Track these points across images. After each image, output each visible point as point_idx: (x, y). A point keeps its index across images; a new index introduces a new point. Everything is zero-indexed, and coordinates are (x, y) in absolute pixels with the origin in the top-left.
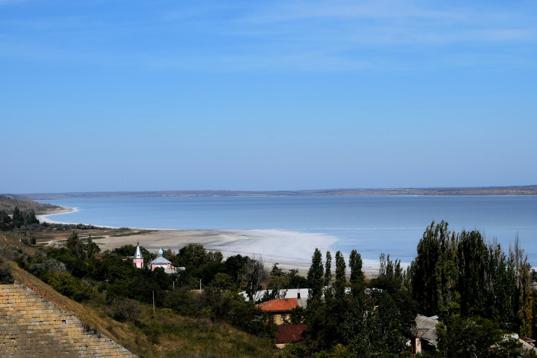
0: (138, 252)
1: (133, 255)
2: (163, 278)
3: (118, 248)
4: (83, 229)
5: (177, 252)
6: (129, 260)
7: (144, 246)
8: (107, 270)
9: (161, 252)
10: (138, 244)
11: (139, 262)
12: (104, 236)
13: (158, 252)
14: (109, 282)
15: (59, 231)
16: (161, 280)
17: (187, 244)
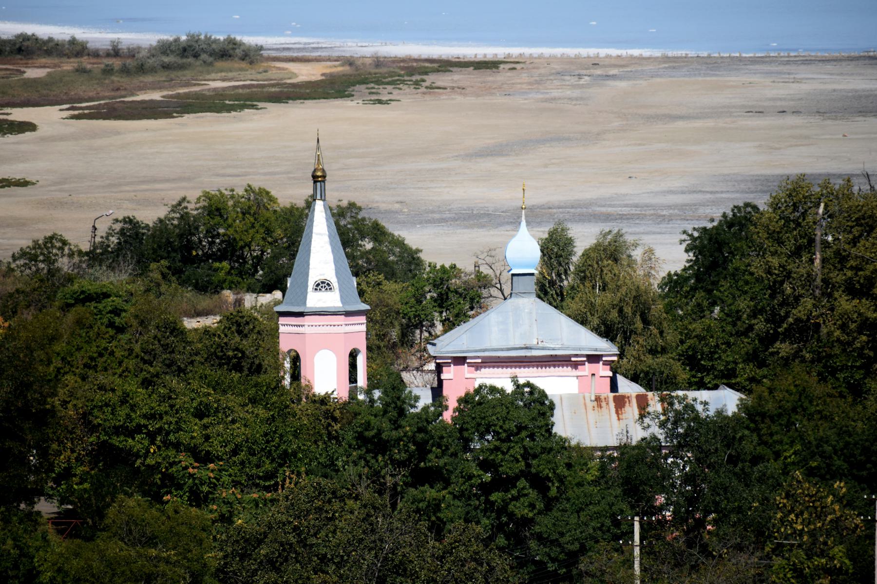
0: (321, 256)
1: (276, 282)
2: (539, 483)
3: (149, 216)
5: (671, 257)
6: (239, 323)
7: (376, 199)
8: (44, 418)
9: (524, 250)
10: (318, 179)
11: (325, 342)
12: (18, 114)
13: (494, 253)
14: (61, 522)
16: (520, 509)
17: (762, 181)
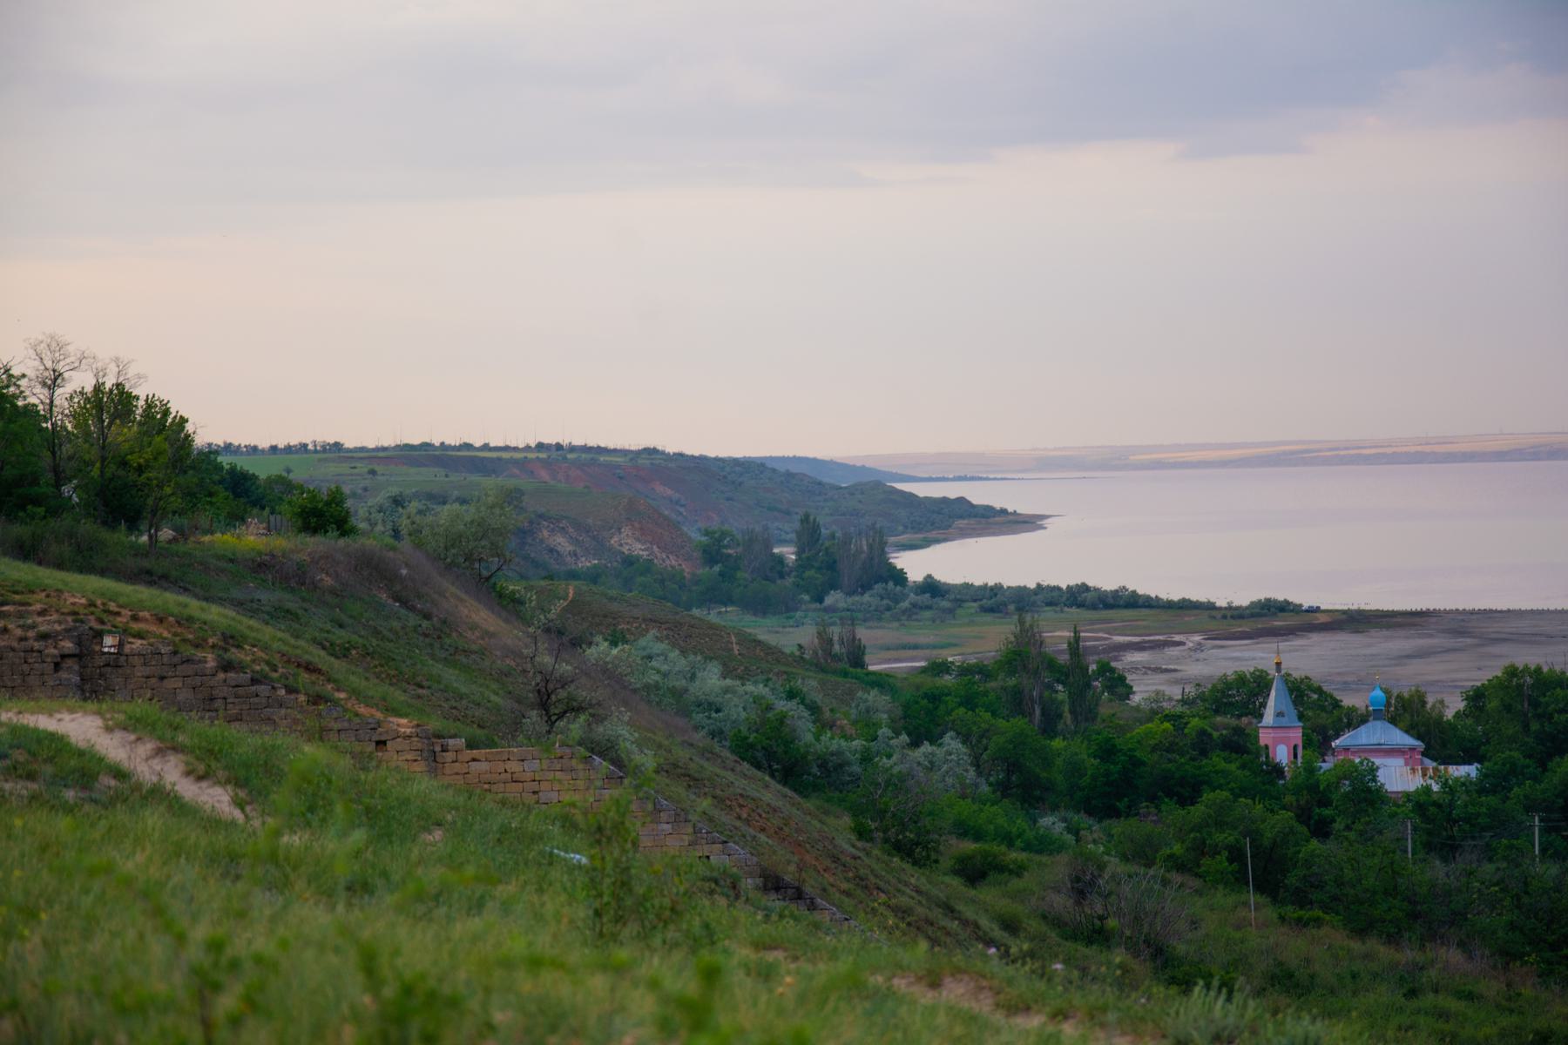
4: (1094, 607)
6: (1239, 731)
15: (988, 618)
